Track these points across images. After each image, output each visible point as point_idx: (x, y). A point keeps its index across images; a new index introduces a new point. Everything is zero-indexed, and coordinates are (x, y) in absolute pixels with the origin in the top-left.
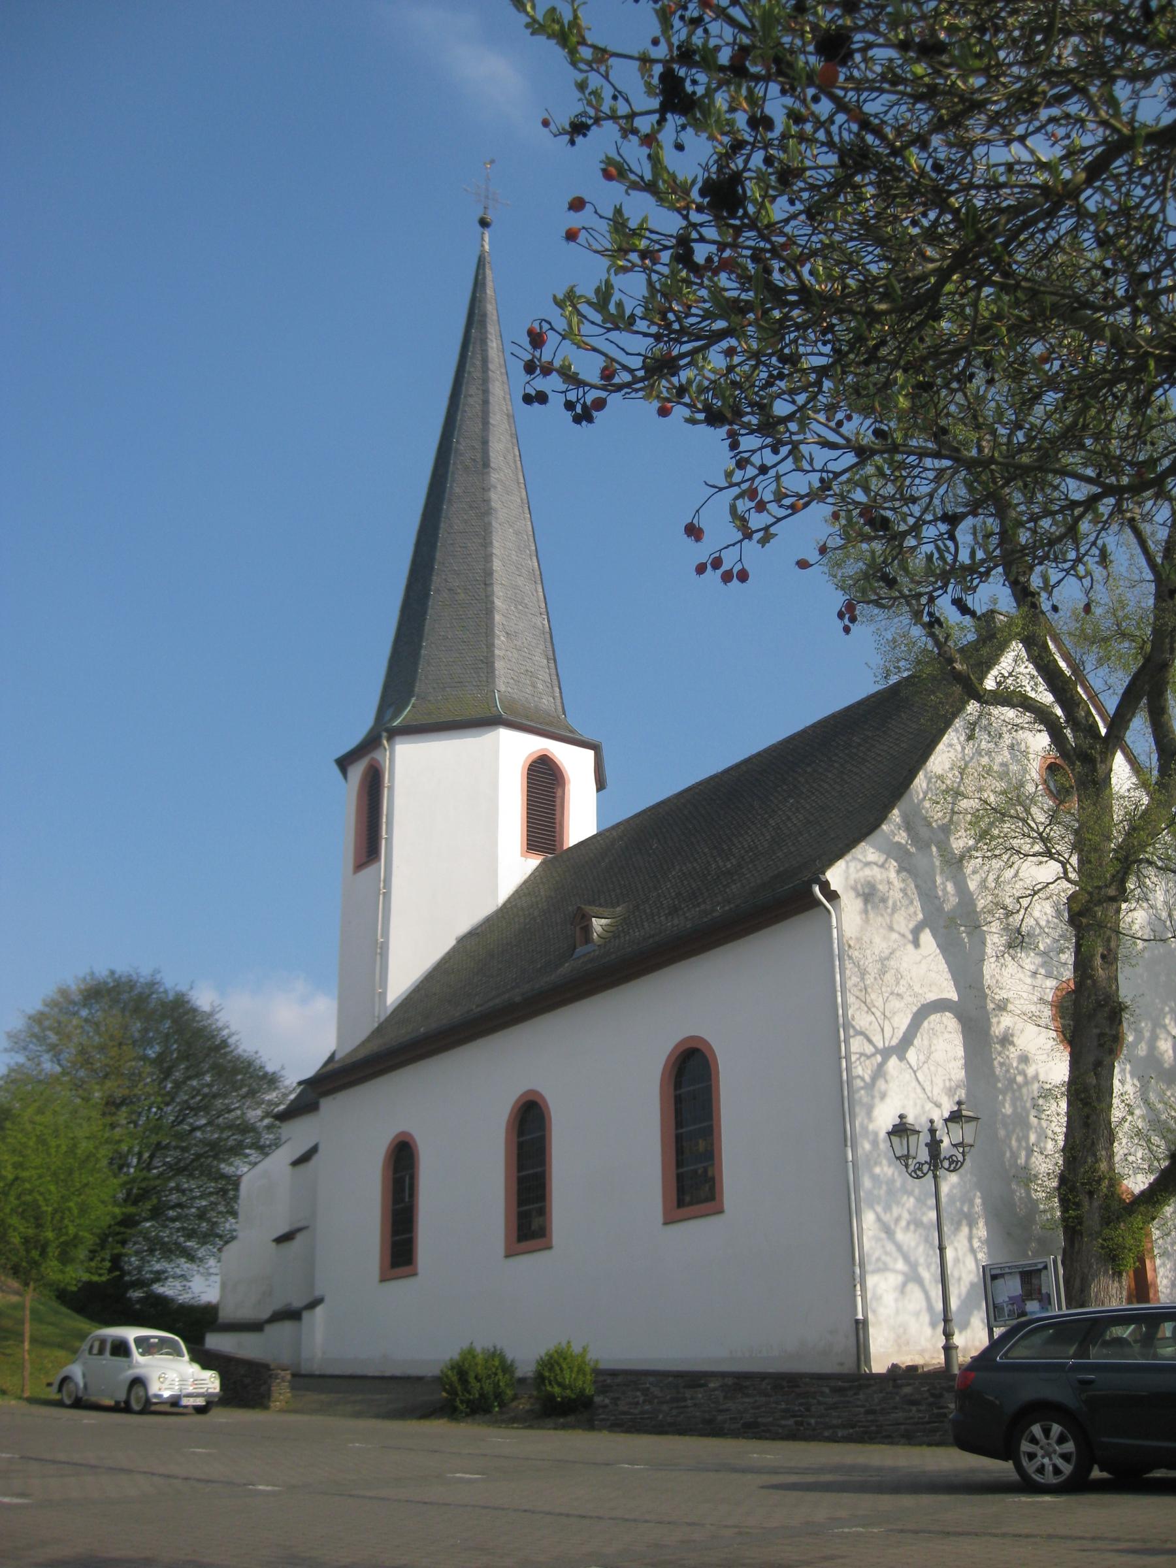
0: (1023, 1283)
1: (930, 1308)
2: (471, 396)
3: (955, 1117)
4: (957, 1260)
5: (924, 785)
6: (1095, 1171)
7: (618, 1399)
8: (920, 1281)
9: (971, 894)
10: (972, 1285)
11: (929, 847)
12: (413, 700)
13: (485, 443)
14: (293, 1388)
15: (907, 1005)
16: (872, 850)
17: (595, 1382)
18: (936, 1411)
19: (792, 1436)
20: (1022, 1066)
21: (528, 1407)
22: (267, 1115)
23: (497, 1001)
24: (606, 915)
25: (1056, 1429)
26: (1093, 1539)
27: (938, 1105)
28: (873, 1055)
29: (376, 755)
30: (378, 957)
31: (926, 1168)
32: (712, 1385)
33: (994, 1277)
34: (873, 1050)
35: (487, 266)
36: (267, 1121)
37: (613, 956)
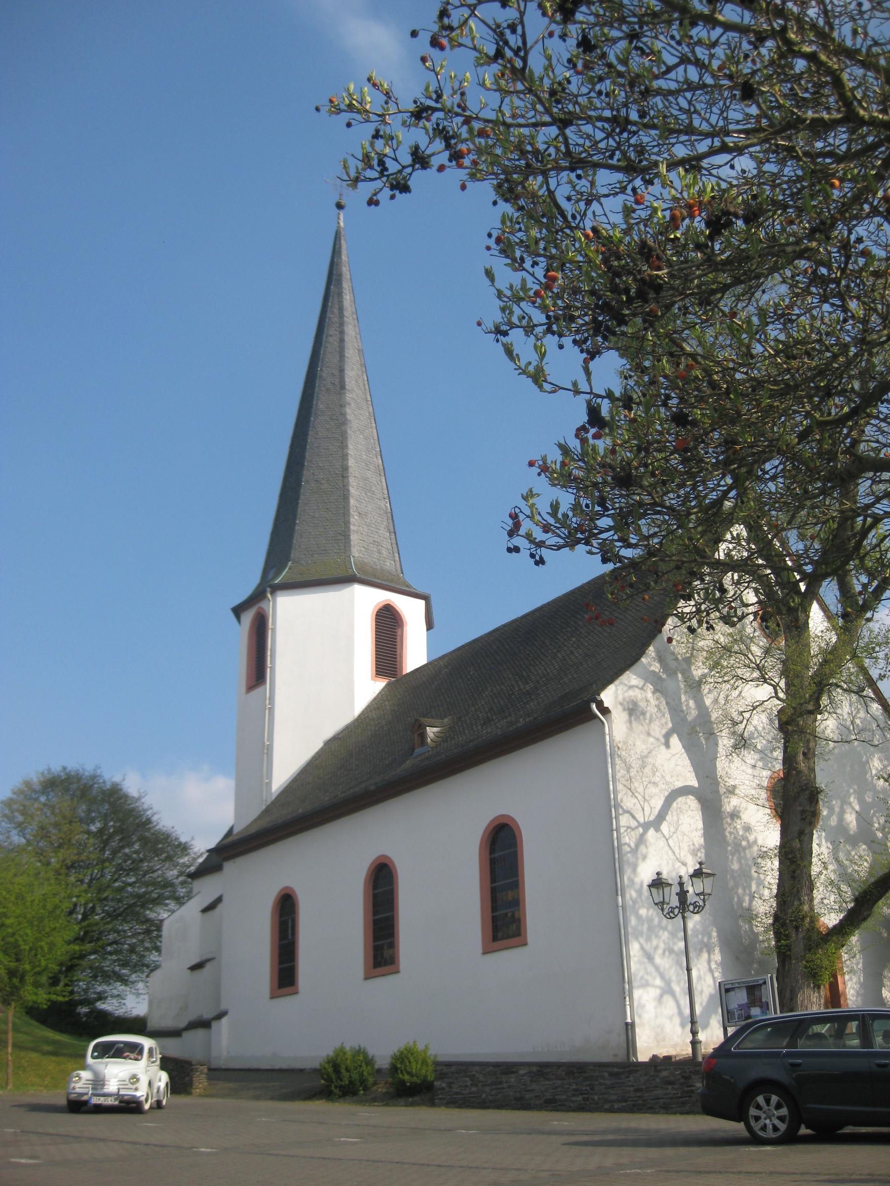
1: (680, 1013)
2: (331, 336)
3: (697, 874)
4: (699, 978)
7: (451, 1083)
8: (672, 994)
9: (707, 708)
10: (711, 996)
12: (290, 564)
13: (342, 371)
14: (209, 1079)
15: (661, 791)
16: (634, 677)
18: (686, 1089)
21: (384, 1090)
22: (181, 874)
24: (436, 724)
25: (774, 1099)
26: (802, 1174)
27: (684, 864)
28: (636, 828)
29: (263, 604)
30: (265, 756)
31: (676, 911)
32: (522, 1072)
33: (727, 991)
35: (342, 238)
36: (181, 879)
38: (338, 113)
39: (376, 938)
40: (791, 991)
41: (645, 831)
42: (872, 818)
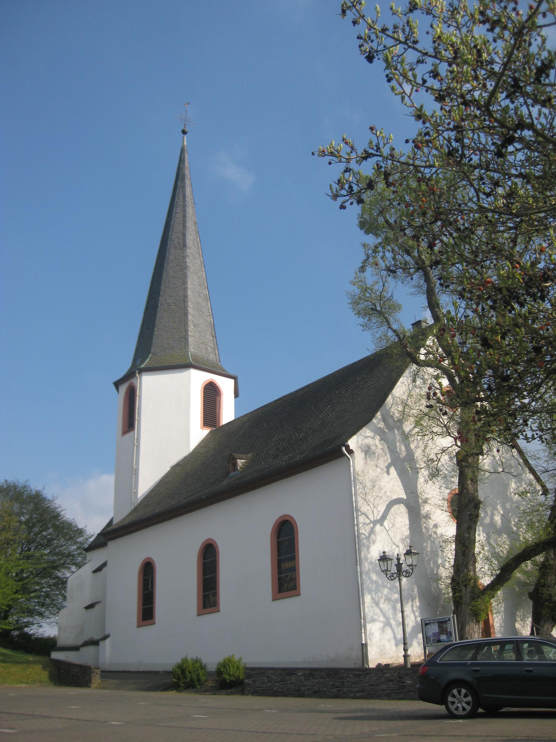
0: (439, 627)
1: (395, 638)
2: (178, 213)
4: (395, 614)
5: (391, 401)
6: (468, 575)
7: (255, 681)
8: (390, 626)
9: (412, 450)
10: (413, 627)
11: (393, 429)
12: (150, 355)
13: (184, 235)
14: (101, 678)
16: (368, 431)
17: (245, 673)
18: (401, 684)
19: (336, 696)
20: (434, 530)
22: (78, 548)
23: (193, 497)
24: (244, 457)
25: (463, 691)
26: (486, 736)
28: (369, 524)
29: (133, 380)
30: (134, 475)
31: (395, 575)
32: (299, 674)
33: (426, 624)
34: (369, 521)
35: (185, 152)
36: (78, 551)
37: (248, 478)
38: (324, 156)
39: (205, 590)
40: (462, 624)
41: (375, 525)
42: (510, 518)
